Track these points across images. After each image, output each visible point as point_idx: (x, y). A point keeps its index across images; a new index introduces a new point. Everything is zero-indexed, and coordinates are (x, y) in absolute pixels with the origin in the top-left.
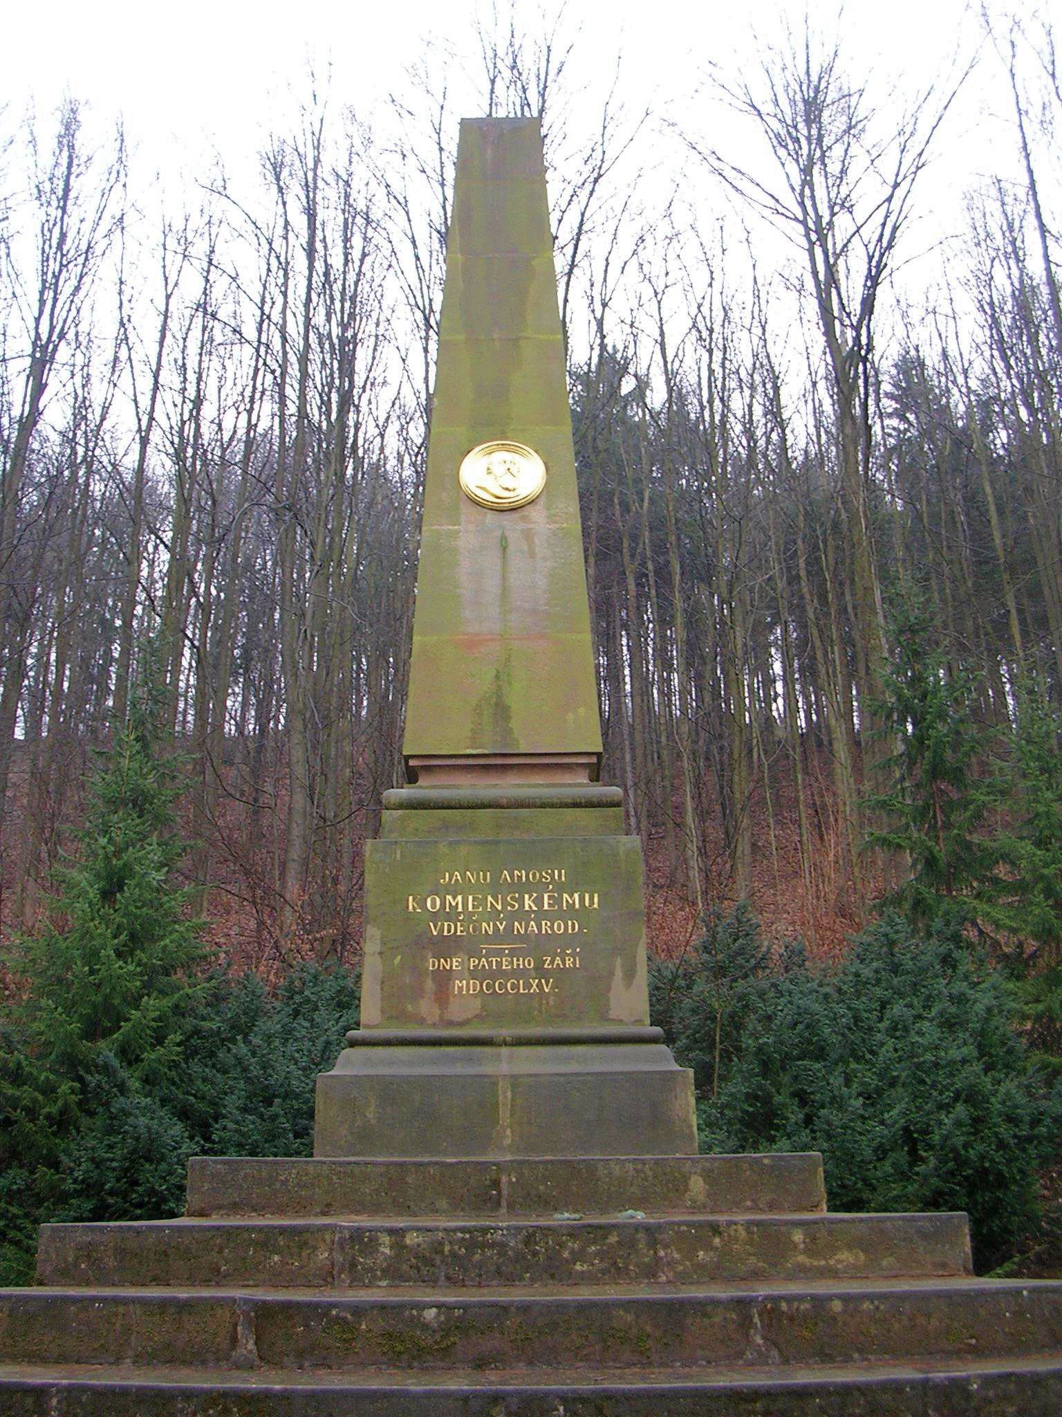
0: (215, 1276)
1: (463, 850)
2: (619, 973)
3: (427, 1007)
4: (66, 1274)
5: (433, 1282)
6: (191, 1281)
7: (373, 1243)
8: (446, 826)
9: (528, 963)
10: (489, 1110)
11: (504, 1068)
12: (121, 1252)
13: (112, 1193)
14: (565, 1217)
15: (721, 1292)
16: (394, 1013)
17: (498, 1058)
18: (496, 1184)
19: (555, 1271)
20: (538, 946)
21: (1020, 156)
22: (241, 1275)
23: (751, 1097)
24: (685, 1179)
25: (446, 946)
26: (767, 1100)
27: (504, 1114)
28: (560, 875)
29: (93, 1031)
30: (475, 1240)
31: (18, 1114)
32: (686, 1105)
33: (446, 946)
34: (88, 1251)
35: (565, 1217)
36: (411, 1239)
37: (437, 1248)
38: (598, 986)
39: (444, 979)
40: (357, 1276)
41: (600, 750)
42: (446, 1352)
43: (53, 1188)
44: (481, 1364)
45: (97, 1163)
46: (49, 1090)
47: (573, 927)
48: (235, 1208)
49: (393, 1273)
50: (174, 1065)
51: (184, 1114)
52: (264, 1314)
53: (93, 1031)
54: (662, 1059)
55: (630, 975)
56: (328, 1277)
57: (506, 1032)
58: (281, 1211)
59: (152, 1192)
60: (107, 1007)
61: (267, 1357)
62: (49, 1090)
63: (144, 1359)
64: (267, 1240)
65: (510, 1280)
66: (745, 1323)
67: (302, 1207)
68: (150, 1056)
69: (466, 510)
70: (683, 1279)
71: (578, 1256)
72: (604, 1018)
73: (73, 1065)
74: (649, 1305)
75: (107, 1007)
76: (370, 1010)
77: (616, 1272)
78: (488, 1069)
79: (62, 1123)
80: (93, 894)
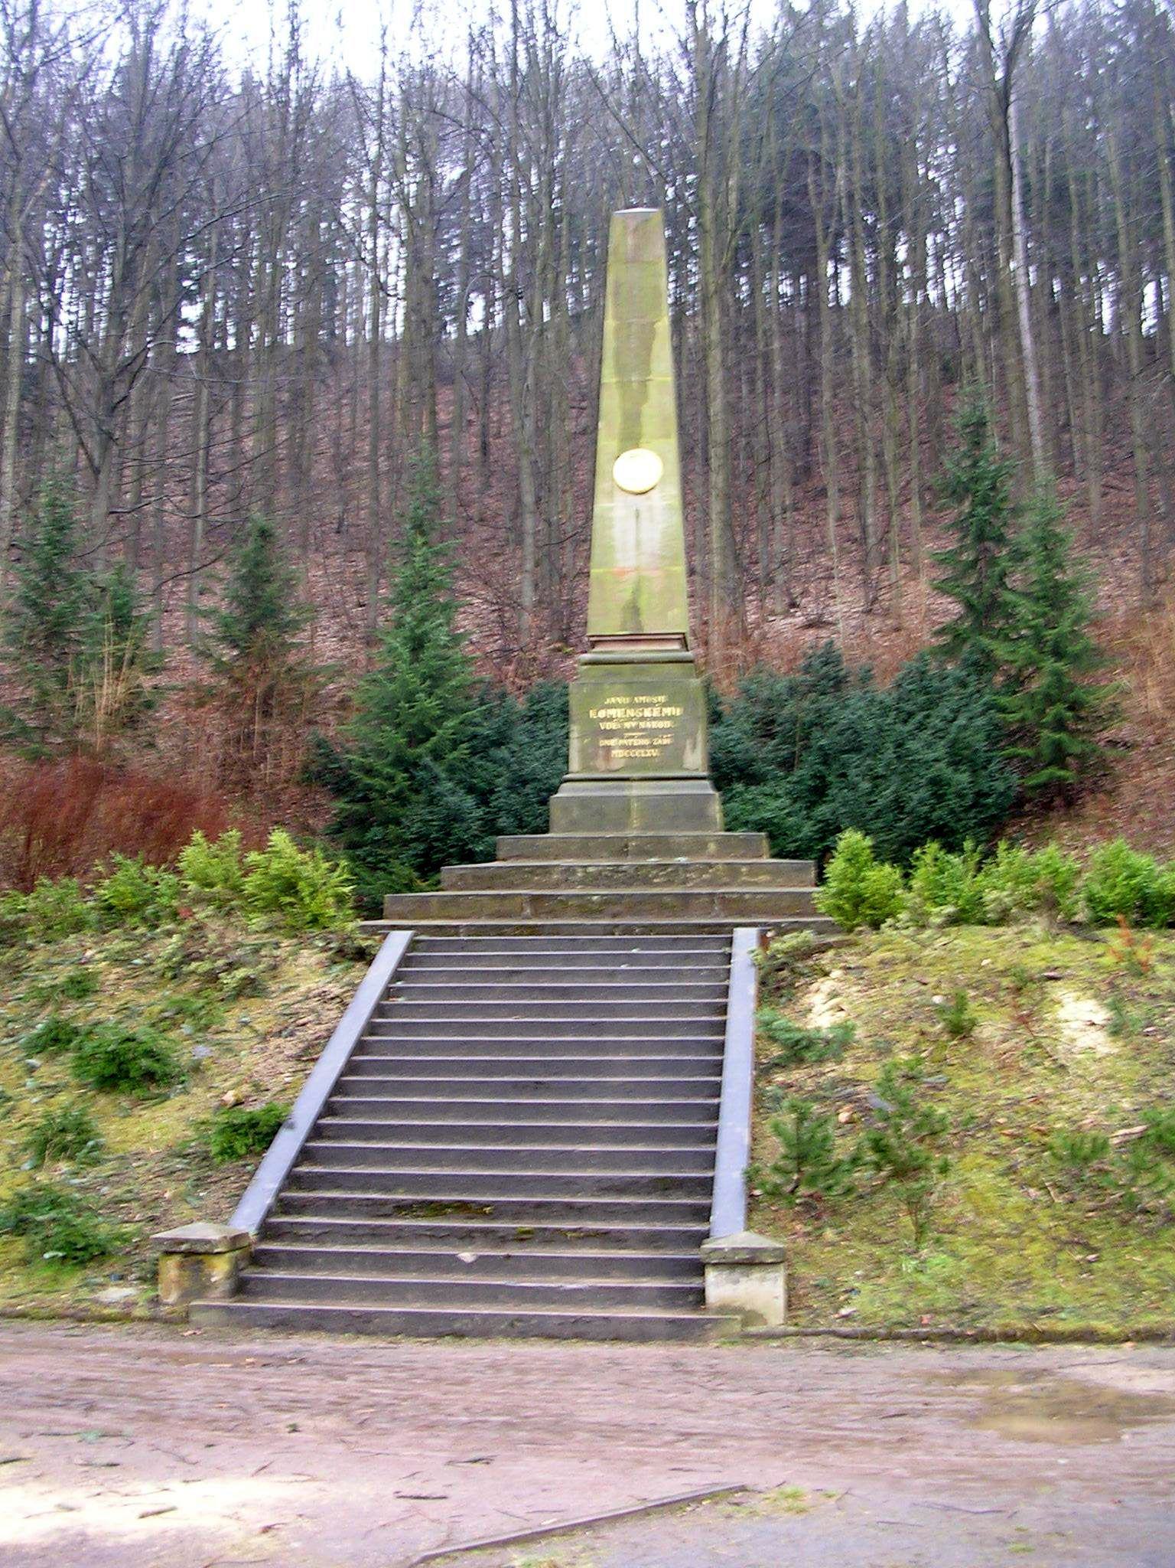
0: (512, 886)
1: (618, 687)
2: (688, 747)
3: (600, 763)
4: (453, 887)
5: (598, 886)
6: (503, 887)
7: (574, 873)
8: (609, 674)
9: (646, 742)
10: (627, 810)
11: (634, 792)
12: (474, 877)
13: (436, 840)
14: (653, 860)
15: (704, 891)
16: (586, 767)
17: (631, 787)
18: (626, 846)
19: (647, 882)
20: (652, 733)
21: (157, 1508)
22: (524, 884)
23: (814, 777)
24: (706, 844)
25: (610, 734)
26: (822, 778)
27: (634, 815)
28: (662, 699)
29: (414, 740)
30: (616, 870)
31: (374, 795)
32: (716, 810)
33: (610, 734)
34: (462, 877)
35: (653, 860)
36: (590, 870)
37: (600, 873)
38: (675, 754)
39: (608, 749)
40: (572, 885)
41: (684, 628)
42: (601, 912)
43: (398, 837)
44: (614, 916)
45: (426, 822)
46: (391, 778)
47: (667, 724)
48: (518, 857)
49: (583, 883)
50: (464, 760)
51: (471, 790)
52: (535, 899)
53: (414, 740)
54: (706, 788)
55: (694, 747)
56: (557, 885)
57: (636, 775)
58: (538, 857)
59: (459, 839)
60: (421, 726)
61: (536, 914)
62: (391, 778)
63: (491, 916)
64: (533, 870)
65: (629, 885)
66: (713, 902)
67: (546, 857)
68: (450, 756)
69: (618, 495)
70: (696, 885)
71: (656, 877)
72: (681, 768)
73: (402, 762)
74: (676, 895)
75: (421, 726)
76: (575, 764)
77: (669, 883)
78: (626, 793)
79: (401, 799)
80: (406, 653)
